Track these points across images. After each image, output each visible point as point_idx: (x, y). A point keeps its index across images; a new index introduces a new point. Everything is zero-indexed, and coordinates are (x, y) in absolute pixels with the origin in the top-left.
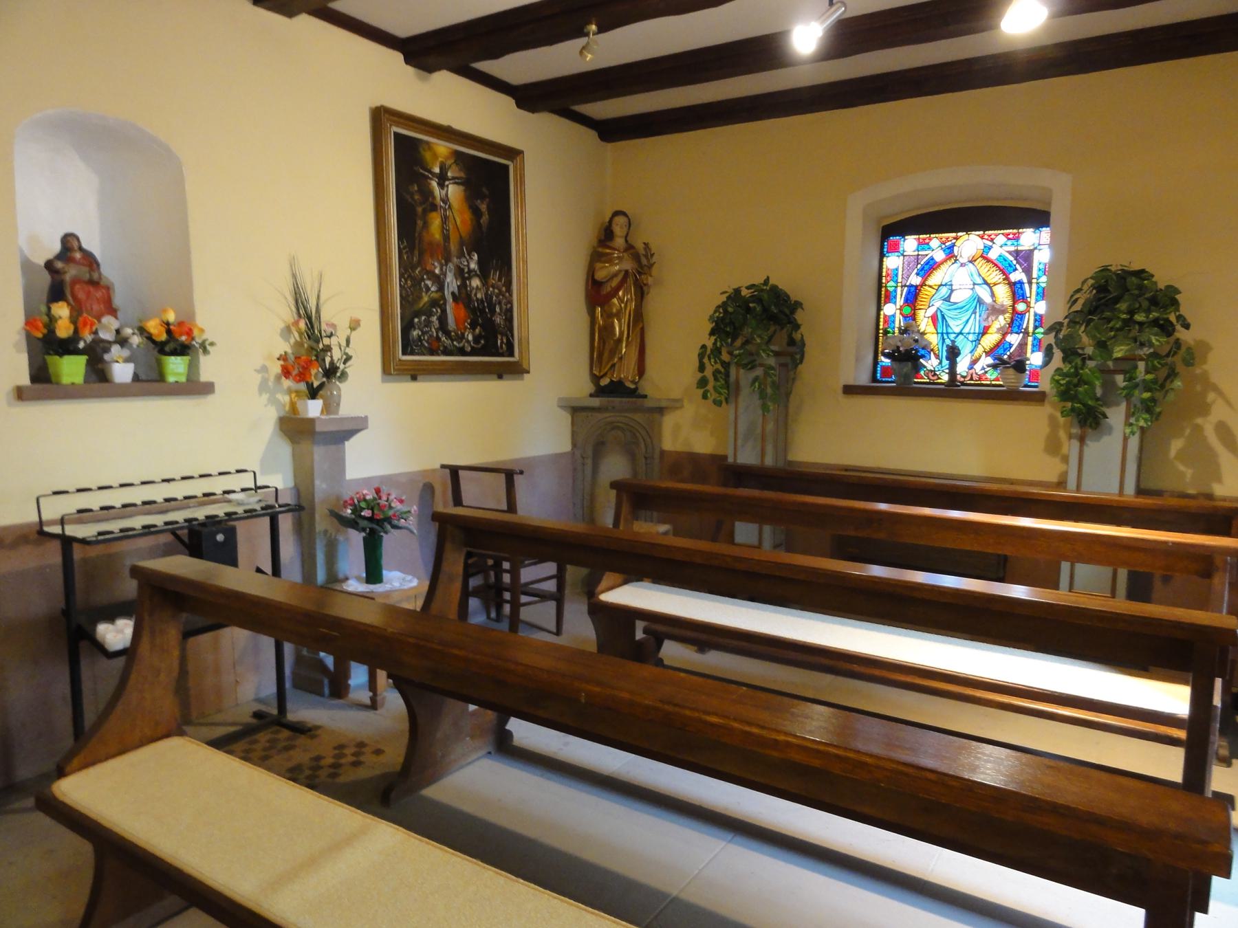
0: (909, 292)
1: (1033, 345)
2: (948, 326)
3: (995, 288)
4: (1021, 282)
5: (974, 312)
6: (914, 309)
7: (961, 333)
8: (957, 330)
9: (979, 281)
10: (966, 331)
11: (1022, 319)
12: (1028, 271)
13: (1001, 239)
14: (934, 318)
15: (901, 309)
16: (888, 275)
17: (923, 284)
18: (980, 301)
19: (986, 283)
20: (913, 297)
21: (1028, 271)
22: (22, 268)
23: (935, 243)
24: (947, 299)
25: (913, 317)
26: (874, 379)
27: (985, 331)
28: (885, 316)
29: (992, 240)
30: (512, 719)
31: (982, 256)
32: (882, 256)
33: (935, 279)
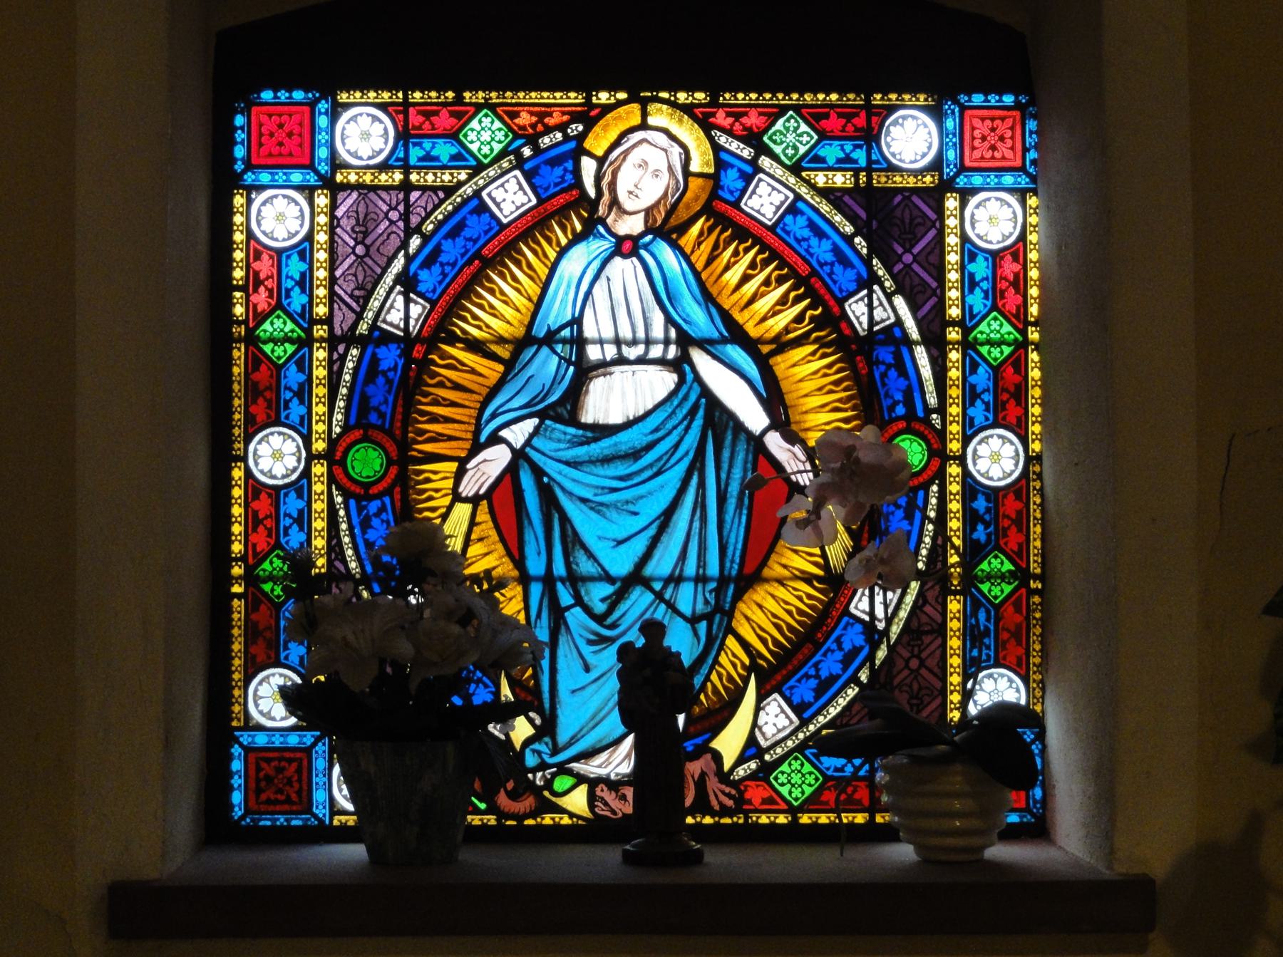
0: (370, 371)
1: (972, 635)
2: (572, 541)
3: (781, 364)
4: (893, 336)
5: (698, 463)
6: (403, 464)
7: (636, 578)
8: (621, 563)
9: (700, 321)
10: (662, 565)
11: (913, 510)
12: (923, 290)
13: (791, 135)
14: (503, 500)
15: (335, 456)
16: (254, 282)
17: (440, 330)
18: (718, 418)
19: (737, 334)
20: (393, 397)
21: (923, 290)
22: (282, 696)
23: (485, 135)
24: (564, 409)
25: (401, 483)
26: (216, 826)
27: (747, 577)
28: (254, 487)
29: (754, 138)
30: (666, 643)
31: (707, 210)
32: (224, 184)
33: (500, 310)
